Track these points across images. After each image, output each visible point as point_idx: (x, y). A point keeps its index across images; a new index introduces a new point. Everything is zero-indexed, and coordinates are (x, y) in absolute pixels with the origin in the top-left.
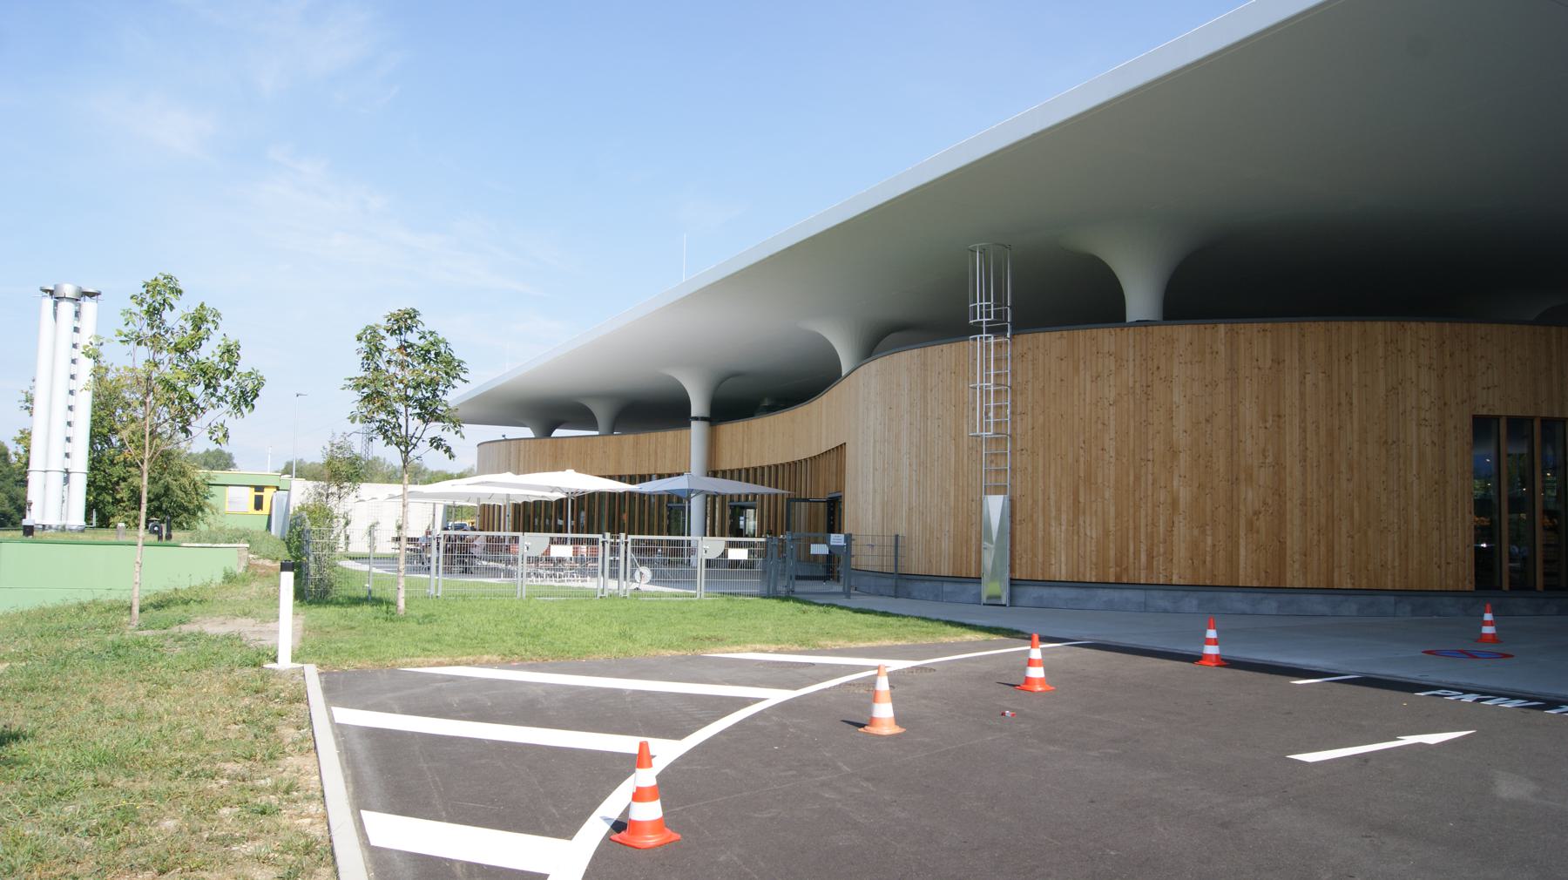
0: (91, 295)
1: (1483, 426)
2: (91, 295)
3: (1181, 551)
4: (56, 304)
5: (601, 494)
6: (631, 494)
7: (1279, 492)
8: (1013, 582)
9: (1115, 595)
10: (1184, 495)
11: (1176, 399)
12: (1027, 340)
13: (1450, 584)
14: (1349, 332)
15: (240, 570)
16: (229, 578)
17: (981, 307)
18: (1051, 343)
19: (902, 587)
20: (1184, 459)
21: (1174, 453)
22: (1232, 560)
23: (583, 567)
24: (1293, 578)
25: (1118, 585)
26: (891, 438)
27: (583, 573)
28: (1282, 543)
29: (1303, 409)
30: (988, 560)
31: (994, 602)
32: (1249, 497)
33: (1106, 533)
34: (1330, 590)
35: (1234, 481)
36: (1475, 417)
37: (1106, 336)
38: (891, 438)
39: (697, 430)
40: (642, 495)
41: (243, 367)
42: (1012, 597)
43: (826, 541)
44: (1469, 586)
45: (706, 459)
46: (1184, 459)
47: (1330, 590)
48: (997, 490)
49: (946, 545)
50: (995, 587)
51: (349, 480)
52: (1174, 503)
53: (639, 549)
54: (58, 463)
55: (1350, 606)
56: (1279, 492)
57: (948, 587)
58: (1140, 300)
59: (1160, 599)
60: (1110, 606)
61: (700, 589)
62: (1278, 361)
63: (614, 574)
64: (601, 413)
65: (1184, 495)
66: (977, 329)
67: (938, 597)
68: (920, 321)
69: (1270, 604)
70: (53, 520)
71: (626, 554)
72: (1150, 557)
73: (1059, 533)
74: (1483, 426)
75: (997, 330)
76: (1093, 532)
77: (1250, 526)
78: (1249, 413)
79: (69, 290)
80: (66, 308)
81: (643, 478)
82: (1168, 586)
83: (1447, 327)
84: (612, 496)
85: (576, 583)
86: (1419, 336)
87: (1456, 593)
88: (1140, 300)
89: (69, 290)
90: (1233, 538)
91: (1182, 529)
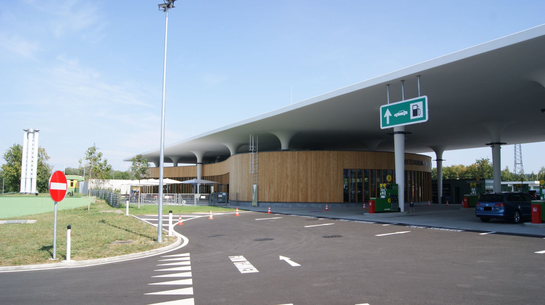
0: (37, 131)
1: (346, 171)
2: (37, 131)
3: (289, 196)
4: (28, 134)
5: (174, 184)
6: (182, 184)
7: (307, 184)
8: (258, 202)
9: (277, 204)
10: (289, 185)
11: (288, 165)
12: (261, 153)
13: (339, 201)
14: (320, 153)
15: (94, 203)
16: (92, 204)
17: (252, 147)
18: (265, 154)
19: (238, 203)
20: (289, 178)
21: (288, 177)
22: (298, 197)
23: (170, 201)
24: (309, 201)
25: (277, 202)
26: (238, 171)
27: (170, 202)
28: (307, 194)
29: (311, 168)
30: (253, 198)
31: (254, 206)
32: (301, 185)
33: (275, 192)
34: (316, 203)
35: (299, 182)
36: (344, 169)
37: (276, 153)
38: (238, 171)
39: (199, 166)
40: (185, 184)
41: (108, 164)
42: (258, 205)
43: (222, 194)
44: (343, 201)
45: (200, 173)
46: (289, 178)
47: (316, 203)
48: (255, 184)
49: (246, 195)
50: (254, 204)
51: (106, 178)
52: (288, 186)
53: (183, 196)
54: (29, 176)
55: (290, 205)
56: (307, 184)
57: (246, 203)
58: (284, 146)
59: (285, 205)
60: (276, 206)
61: (195, 205)
62: (307, 159)
63: (178, 202)
64: (173, 159)
65: (289, 185)
66: (251, 151)
67: (245, 205)
68: (242, 149)
69: (305, 206)
70: (28, 191)
71: (180, 197)
72: (283, 197)
73: (267, 192)
74: (346, 171)
75: (255, 152)
76: (273, 192)
77: (301, 190)
78: (301, 168)
79: (32, 130)
80: (31, 135)
81: (186, 179)
82: (287, 202)
83: (339, 152)
84: (177, 184)
85: (170, 204)
86: (333, 154)
87: (340, 203)
88: (284, 146)
89: (32, 130)
90: (298, 193)
91: (289, 191)
